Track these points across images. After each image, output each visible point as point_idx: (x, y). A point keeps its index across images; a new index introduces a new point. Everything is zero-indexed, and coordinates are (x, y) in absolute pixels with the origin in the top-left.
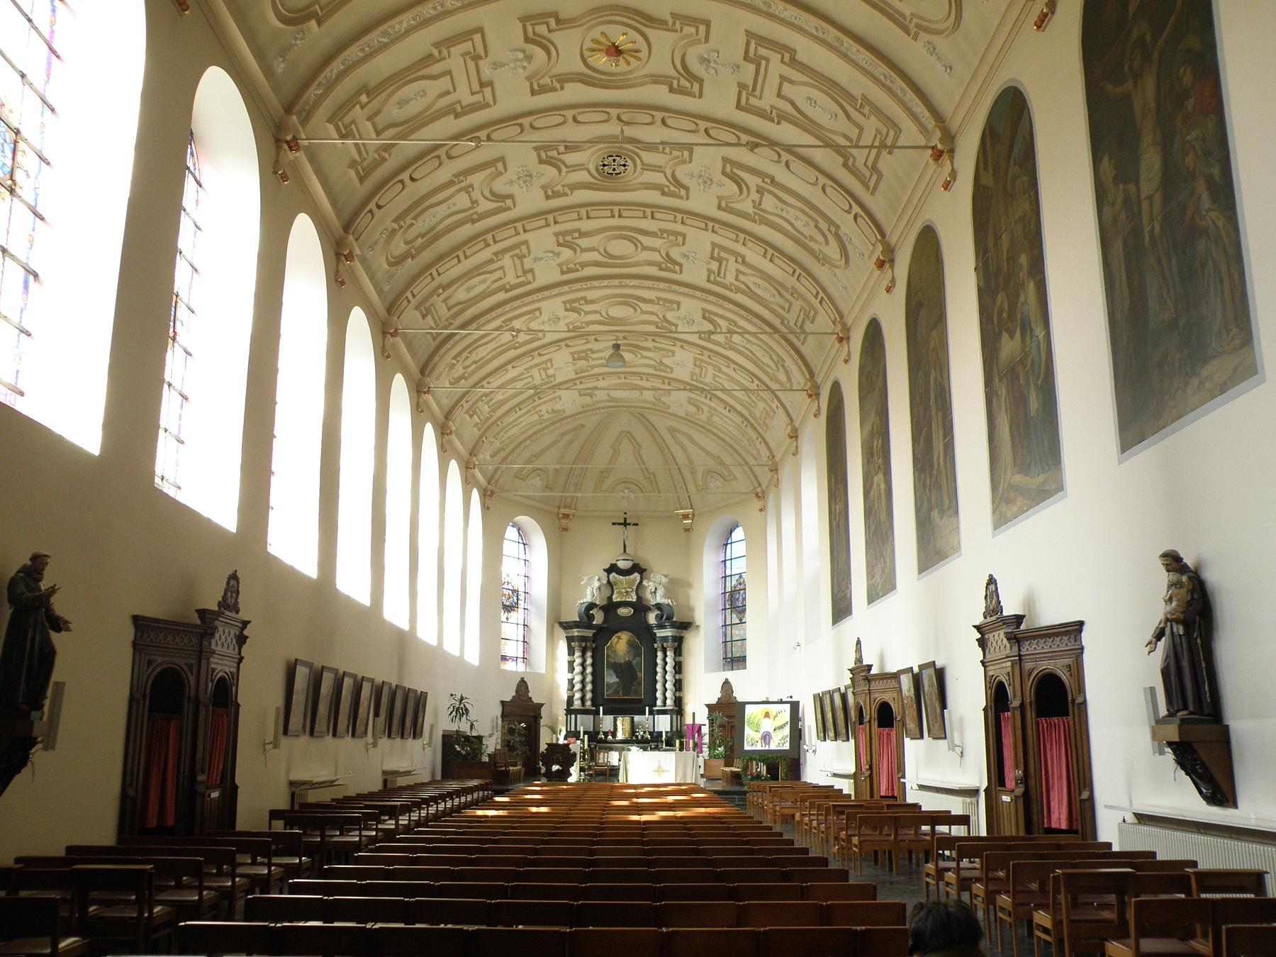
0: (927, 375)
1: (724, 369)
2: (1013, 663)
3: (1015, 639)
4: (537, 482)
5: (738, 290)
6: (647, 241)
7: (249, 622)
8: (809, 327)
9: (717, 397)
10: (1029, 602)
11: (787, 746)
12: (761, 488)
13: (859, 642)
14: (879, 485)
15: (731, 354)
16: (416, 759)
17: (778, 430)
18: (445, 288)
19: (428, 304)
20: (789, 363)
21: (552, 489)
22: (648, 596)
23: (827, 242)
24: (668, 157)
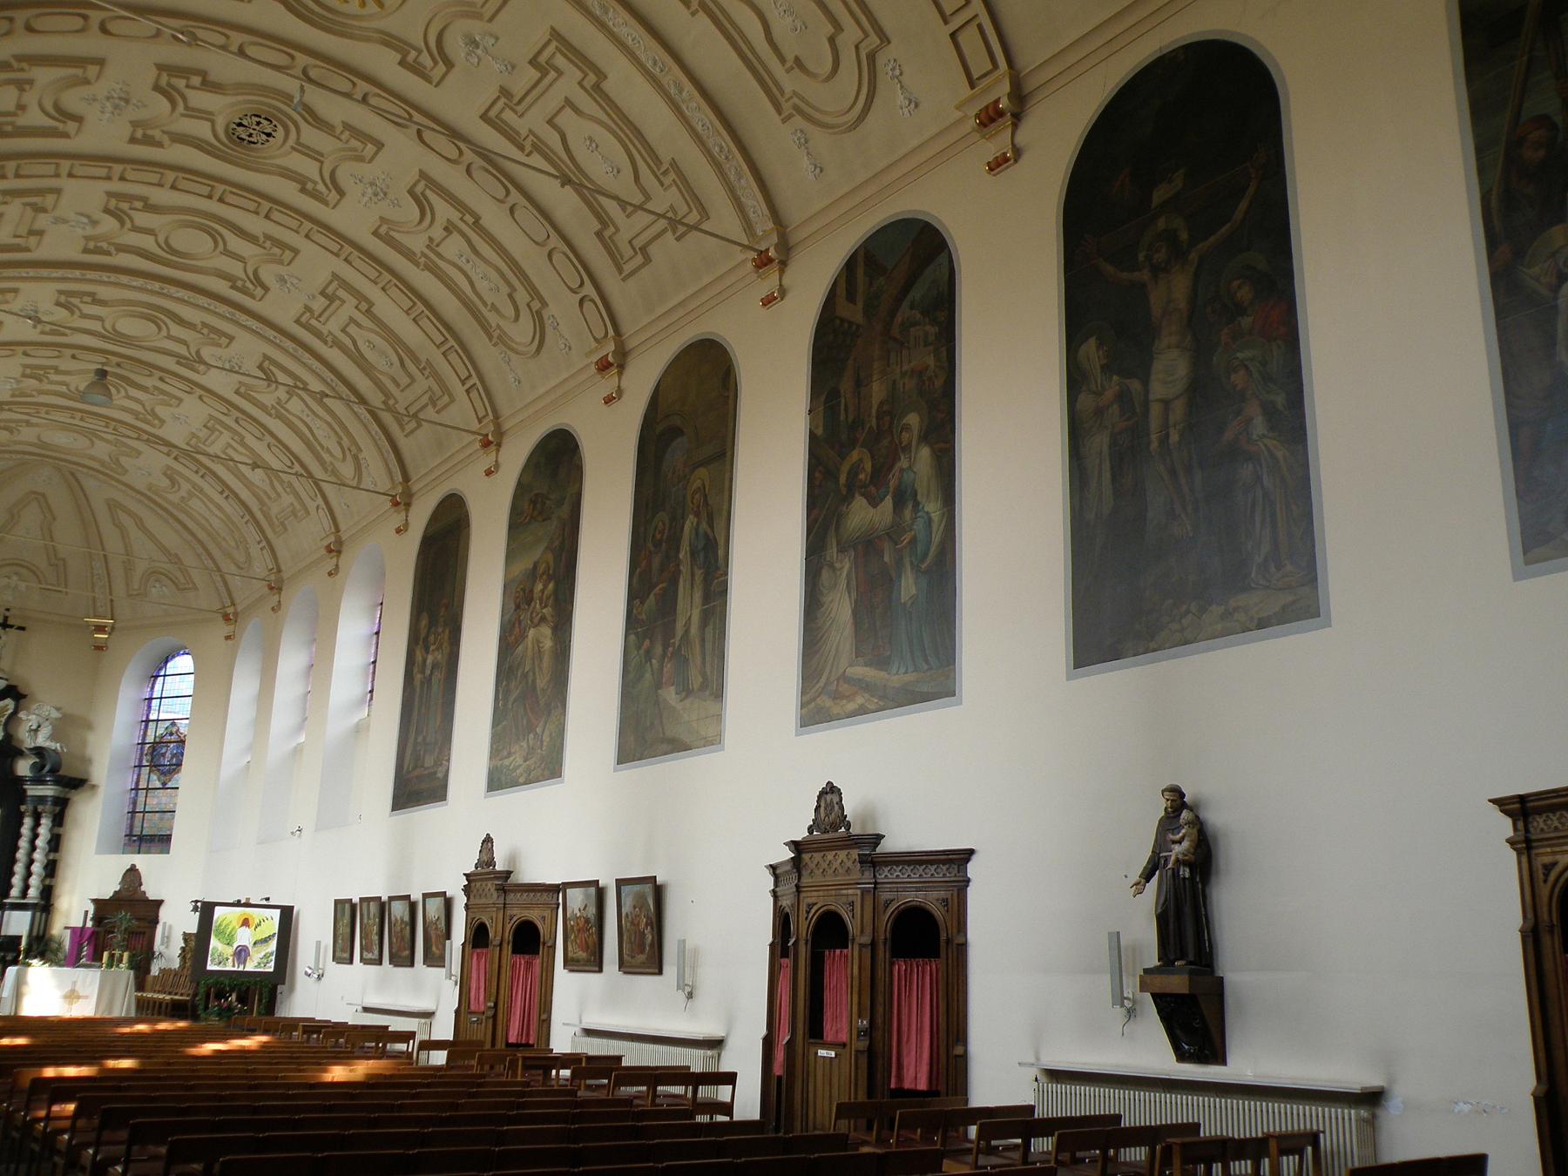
0: (676, 521)
2: (864, 891)
5: (337, 343)
6: (235, 243)
11: (270, 968)
17: (310, 533)
24: (340, 145)
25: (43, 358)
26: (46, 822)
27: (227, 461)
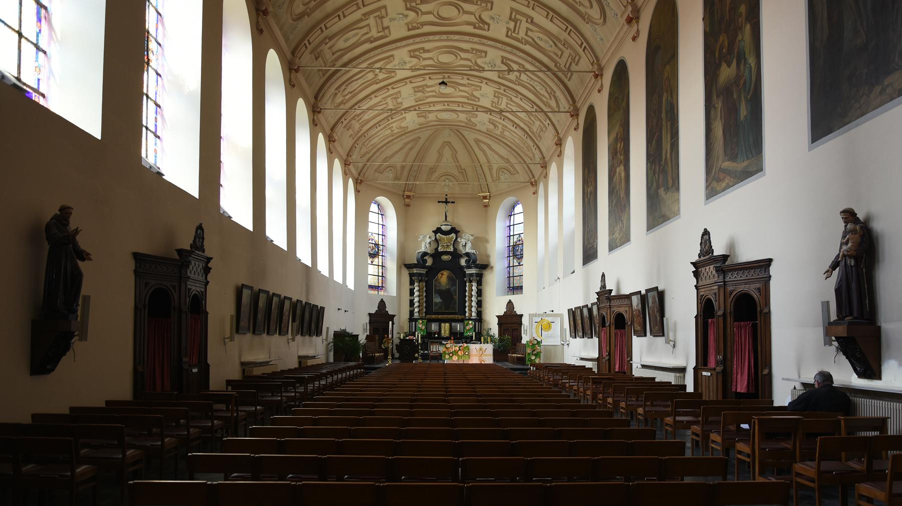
0: (660, 97)
1: (514, 98)
3: (721, 271)
4: (390, 175)
5: (527, 43)
7: (212, 258)
8: (574, 67)
9: (508, 118)
10: (732, 246)
12: (532, 179)
13: (603, 275)
14: (620, 174)
15: (519, 88)
16: (317, 348)
18: (331, 38)
19: (319, 50)
20: (559, 94)
21: (399, 179)
22: (461, 248)
23: (592, 7)
25: (419, 83)
26: (474, 285)
27: (512, 112)
